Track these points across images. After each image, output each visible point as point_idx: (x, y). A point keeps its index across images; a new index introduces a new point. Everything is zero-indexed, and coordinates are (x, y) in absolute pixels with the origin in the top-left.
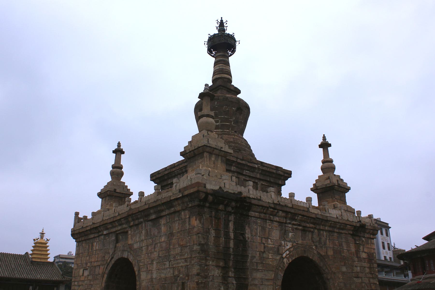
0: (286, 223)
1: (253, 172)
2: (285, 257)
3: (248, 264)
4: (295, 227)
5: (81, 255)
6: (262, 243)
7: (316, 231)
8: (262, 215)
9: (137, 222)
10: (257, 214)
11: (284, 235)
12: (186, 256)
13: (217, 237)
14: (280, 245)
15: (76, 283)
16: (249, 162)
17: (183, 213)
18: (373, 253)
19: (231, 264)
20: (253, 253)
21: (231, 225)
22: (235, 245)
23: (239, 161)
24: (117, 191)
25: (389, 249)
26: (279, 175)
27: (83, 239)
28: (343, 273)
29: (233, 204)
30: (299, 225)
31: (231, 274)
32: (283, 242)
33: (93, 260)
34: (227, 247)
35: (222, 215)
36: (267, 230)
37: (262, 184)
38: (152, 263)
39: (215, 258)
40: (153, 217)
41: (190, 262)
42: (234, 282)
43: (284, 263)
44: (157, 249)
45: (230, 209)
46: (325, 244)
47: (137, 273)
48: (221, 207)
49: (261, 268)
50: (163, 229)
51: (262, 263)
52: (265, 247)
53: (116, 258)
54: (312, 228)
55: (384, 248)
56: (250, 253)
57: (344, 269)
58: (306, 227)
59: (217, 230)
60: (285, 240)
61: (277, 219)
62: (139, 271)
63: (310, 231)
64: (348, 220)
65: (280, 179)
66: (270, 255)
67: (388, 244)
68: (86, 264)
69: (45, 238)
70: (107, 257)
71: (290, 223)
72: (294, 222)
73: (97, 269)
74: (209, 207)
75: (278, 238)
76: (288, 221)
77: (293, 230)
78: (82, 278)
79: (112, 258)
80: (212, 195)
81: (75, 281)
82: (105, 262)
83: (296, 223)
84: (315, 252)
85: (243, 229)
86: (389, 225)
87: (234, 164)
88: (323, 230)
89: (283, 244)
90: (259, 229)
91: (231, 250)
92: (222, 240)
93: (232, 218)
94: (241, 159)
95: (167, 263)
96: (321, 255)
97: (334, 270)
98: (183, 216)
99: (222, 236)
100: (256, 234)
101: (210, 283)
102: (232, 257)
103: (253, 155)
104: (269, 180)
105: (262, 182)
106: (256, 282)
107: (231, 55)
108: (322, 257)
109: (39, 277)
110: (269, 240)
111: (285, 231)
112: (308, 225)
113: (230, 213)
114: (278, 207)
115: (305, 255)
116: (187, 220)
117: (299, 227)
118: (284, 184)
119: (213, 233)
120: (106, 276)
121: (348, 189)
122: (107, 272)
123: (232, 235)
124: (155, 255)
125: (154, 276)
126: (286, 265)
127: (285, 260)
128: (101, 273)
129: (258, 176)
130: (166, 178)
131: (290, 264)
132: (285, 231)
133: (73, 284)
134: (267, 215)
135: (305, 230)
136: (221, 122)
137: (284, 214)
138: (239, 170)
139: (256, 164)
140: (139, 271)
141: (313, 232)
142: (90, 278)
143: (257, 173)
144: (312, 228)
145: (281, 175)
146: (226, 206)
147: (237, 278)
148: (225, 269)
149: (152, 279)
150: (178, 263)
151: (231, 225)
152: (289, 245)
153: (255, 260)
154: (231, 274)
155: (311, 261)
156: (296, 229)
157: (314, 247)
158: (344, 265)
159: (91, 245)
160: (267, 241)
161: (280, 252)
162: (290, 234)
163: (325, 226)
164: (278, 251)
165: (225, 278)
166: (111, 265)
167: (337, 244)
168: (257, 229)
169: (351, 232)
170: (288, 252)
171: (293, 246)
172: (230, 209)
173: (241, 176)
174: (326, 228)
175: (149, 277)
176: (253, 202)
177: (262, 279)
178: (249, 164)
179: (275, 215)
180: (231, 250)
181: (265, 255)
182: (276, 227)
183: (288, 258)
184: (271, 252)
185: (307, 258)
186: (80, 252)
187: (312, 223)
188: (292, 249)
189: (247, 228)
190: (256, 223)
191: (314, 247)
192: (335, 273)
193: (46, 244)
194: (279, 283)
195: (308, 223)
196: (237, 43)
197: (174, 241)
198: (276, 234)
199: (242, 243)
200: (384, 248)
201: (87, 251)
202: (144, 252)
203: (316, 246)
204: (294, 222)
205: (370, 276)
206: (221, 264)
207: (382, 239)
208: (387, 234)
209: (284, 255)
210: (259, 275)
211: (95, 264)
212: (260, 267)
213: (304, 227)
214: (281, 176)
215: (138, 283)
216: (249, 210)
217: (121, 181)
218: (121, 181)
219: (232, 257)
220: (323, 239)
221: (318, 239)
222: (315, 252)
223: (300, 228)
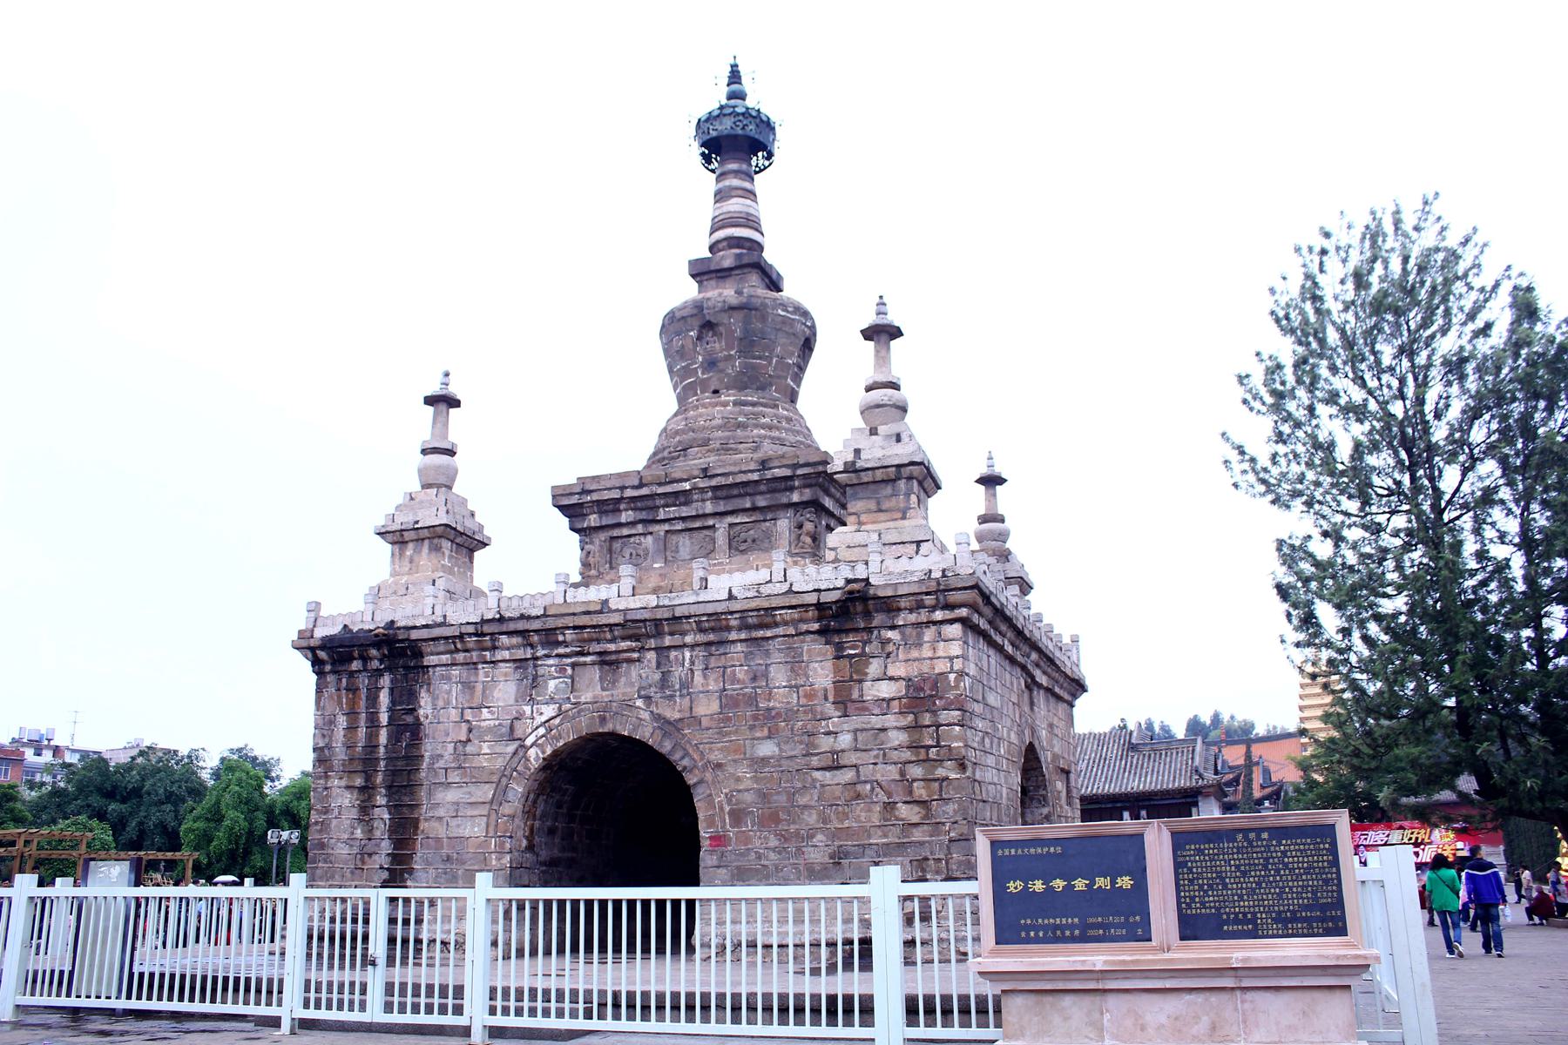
0: (537, 659)
1: (686, 504)
3: (423, 774)
8: (460, 657)
10: (444, 657)
11: (532, 687)
13: (352, 728)
16: (660, 484)
19: (379, 779)
20: (437, 746)
21: (384, 698)
22: (390, 737)
23: (629, 493)
29: (374, 652)
30: (581, 654)
31: (381, 800)
32: (527, 709)
34: (372, 746)
35: (363, 681)
36: (479, 687)
39: (790, 687)
42: (387, 816)
45: (375, 664)
46: (686, 685)
48: (356, 665)
51: (460, 767)
52: (470, 731)
54: (632, 650)
56: (428, 749)
57: (767, 749)
59: (352, 714)
61: (506, 654)
64: (790, 591)
71: (548, 656)
72: (561, 650)
74: (333, 672)
75: (512, 701)
76: (540, 653)
80: (322, 648)
83: (568, 650)
84: (645, 715)
85: (412, 696)
87: (622, 506)
89: (528, 712)
90: (455, 689)
91: (382, 750)
92: (362, 732)
93: (386, 681)
94: (634, 487)
96: (668, 722)
97: (716, 756)
99: (362, 723)
100: (448, 702)
101: (334, 822)
102: (382, 763)
103: (807, 433)
104: (748, 505)
106: (441, 812)
108: (668, 726)
111: (535, 678)
112: (612, 647)
113: (378, 673)
114: (487, 629)
115: (608, 728)
117: (583, 659)
119: (342, 721)
121: (484, 544)
123: (384, 718)
127: (532, 753)
129: (709, 507)
132: (535, 678)
134: (474, 654)
135: (608, 663)
137: (516, 640)
138: (643, 515)
139: (686, 480)
143: (703, 500)
144: (632, 650)
146: (365, 659)
147: (394, 808)
148: (367, 790)
151: (384, 698)
153: (441, 764)
154: (381, 800)
156: (573, 665)
161: (518, 733)
162: (552, 684)
163: (683, 633)
165: (365, 809)
169: (816, 626)
170: (542, 731)
174: (689, 639)
176: (414, 635)
178: (660, 490)
179: (494, 648)
180: (382, 750)
181: (469, 749)
182: (506, 675)
183: (541, 746)
185: (613, 735)
187: (624, 638)
188: (557, 721)
189: (423, 694)
190: (448, 678)
192: (719, 766)
195: (611, 641)
199: (408, 730)
204: (561, 650)
205: (907, 755)
206: (359, 781)
210: (451, 796)
213: (600, 654)
216: (421, 655)
219: (382, 763)
220: (678, 673)
221: (657, 676)
223: (589, 659)
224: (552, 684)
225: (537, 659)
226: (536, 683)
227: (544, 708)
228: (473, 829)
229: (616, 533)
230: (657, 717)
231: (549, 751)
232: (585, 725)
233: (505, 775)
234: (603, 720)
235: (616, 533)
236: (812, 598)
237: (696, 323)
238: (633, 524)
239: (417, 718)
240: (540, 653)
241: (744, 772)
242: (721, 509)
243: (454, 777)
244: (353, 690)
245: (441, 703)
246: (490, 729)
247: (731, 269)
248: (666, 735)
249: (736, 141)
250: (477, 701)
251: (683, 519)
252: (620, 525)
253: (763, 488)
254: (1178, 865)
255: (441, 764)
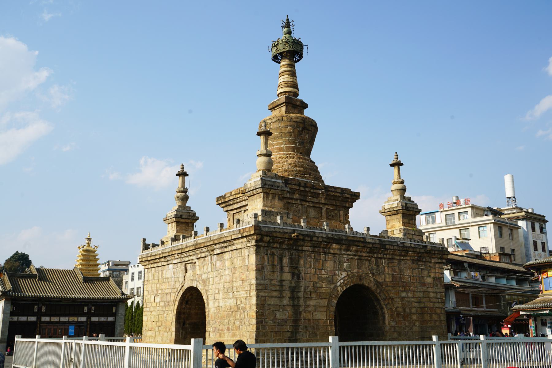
0: (341, 254)
1: (316, 198)
2: (340, 286)
4: (350, 257)
5: (150, 281)
6: (315, 273)
7: (373, 259)
9: (203, 255)
12: (246, 289)
14: (335, 274)
15: (148, 309)
17: (243, 251)
18: (441, 278)
23: (302, 188)
24: (183, 217)
25: (544, 250)
26: (346, 198)
27: (152, 266)
28: (402, 299)
30: (355, 255)
32: (337, 272)
33: (163, 287)
36: (321, 262)
37: (327, 209)
38: (219, 293)
40: (218, 251)
41: (250, 294)
43: (338, 291)
44: (222, 281)
47: (205, 301)
49: (315, 297)
50: (227, 263)
51: (315, 292)
53: (186, 287)
55: (536, 248)
58: (362, 256)
60: (339, 270)
62: (207, 299)
63: (367, 260)
65: (346, 202)
66: (324, 284)
67: (543, 244)
68: (157, 291)
69: (92, 244)
70: (178, 286)
71: (344, 254)
72: (349, 253)
73: (168, 296)
77: (348, 260)
78: (154, 305)
79: (182, 286)
81: (146, 307)
82: (176, 290)
84: (372, 279)
86: (546, 219)
88: (381, 258)
89: (338, 274)
95: (231, 294)
97: (392, 295)
98: (243, 254)
105: (327, 207)
107: (298, 61)
109: (94, 296)
110: (323, 271)
116: (246, 257)
118: (352, 207)
120: (177, 303)
122: (178, 299)
124: (221, 285)
125: (221, 305)
126: (340, 293)
128: (172, 300)
130: (231, 203)
131: (344, 292)
133: (144, 310)
136: (285, 144)
140: (207, 299)
141: (370, 261)
142: (162, 304)
144: (369, 257)
145: (348, 198)
149: (218, 308)
150: (239, 295)
152: (344, 274)
153: (308, 290)
155: (367, 288)
156: (351, 258)
157: (370, 275)
158: (404, 291)
159: (160, 273)
160: (321, 272)
161: (335, 281)
162: (345, 264)
164: (331, 281)
166: (181, 293)
167: (397, 270)
168: (310, 262)
170: (342, 281)
171: (348, 275)
172: (284, 247)
173: (304, 203)
175: (216, 305)
177: (315, 306)
183: (342, 287)
184: (325, 282)
186: (150, 279)
188: (346, 278)
191: (370, 275)
192: (393, 299)
193: (94, 252)
194: (333, 309)
195: (364, 252)
196: (305, 47)
197: (236, 275)
198: (329, 265)
200: (536, 248)
201: (156, 278)
202: (211, 283)
203: (373, 274)
204: (349, 253)
207: (533, 237)
208: (542, 230)
209: (339, 284)
211: (167, 291)
212: (314, 296)
213: (359, 256)
214: (346, 198)
215: (207, 310)
217: (187, 205)
218: (187, 205)
222: (372, 279)
223: (356, 257)
224: (345, 264)
225: (341, 254)
226: (341, 263)
227: (343, 273)
228: (321, 316)
229: (290, 201)
230: (376, 281)
231: (345, 288)
232: (356, 281)
233: (330, 297)
234: (360, 279)
235: (290, 201)
236: (370, 246)
237: (301, 126)
238: (296, 200)
239: (299, 271)
240: (343, 252)
241: (398, 300)
242: (326, 202)
243: (314, 296)
244: (273, 255)
245: (308, 266)
246: (325, 278)
247: (298, 106)
248: (378, 287)
249: (291, 52)
250: (320, 267)
251: (313, 202)
252: (292, 199)
253: (340, 199)
254: (389, 340)
255: (308, 290)
